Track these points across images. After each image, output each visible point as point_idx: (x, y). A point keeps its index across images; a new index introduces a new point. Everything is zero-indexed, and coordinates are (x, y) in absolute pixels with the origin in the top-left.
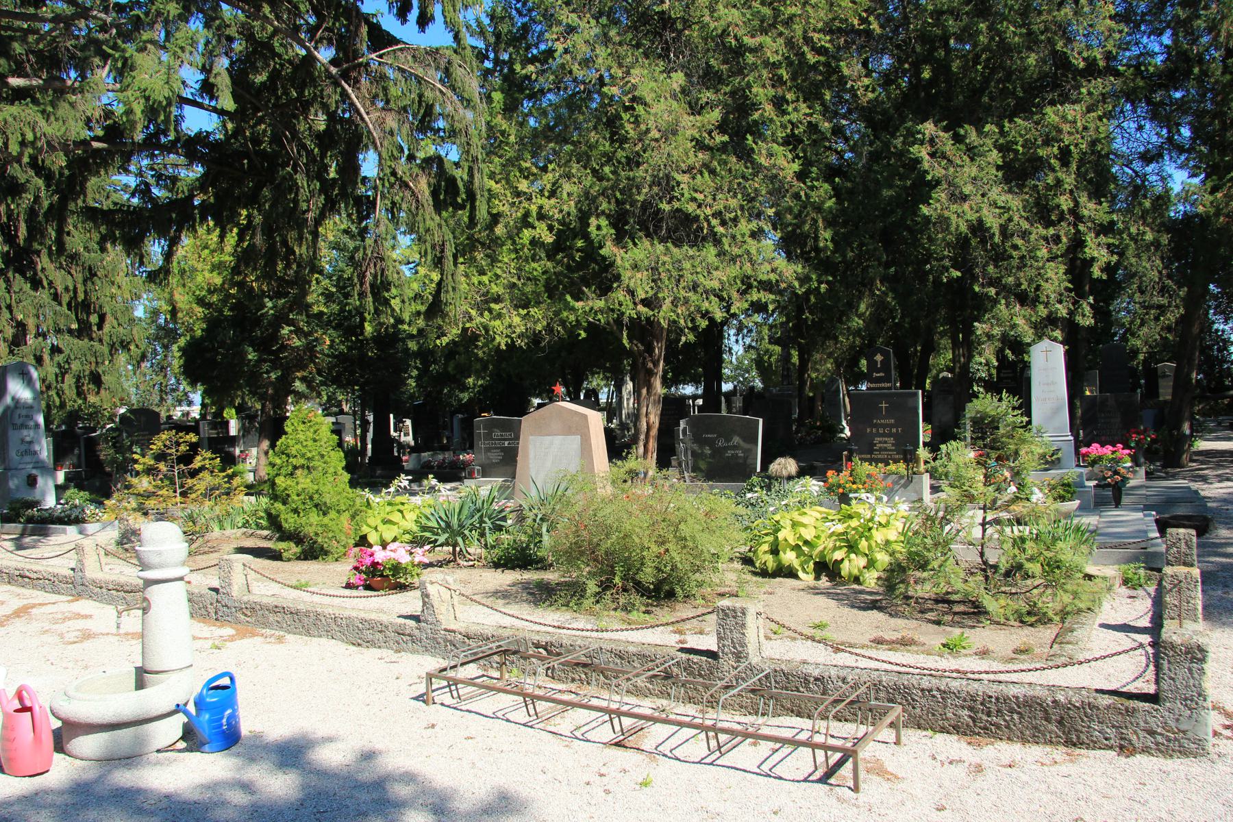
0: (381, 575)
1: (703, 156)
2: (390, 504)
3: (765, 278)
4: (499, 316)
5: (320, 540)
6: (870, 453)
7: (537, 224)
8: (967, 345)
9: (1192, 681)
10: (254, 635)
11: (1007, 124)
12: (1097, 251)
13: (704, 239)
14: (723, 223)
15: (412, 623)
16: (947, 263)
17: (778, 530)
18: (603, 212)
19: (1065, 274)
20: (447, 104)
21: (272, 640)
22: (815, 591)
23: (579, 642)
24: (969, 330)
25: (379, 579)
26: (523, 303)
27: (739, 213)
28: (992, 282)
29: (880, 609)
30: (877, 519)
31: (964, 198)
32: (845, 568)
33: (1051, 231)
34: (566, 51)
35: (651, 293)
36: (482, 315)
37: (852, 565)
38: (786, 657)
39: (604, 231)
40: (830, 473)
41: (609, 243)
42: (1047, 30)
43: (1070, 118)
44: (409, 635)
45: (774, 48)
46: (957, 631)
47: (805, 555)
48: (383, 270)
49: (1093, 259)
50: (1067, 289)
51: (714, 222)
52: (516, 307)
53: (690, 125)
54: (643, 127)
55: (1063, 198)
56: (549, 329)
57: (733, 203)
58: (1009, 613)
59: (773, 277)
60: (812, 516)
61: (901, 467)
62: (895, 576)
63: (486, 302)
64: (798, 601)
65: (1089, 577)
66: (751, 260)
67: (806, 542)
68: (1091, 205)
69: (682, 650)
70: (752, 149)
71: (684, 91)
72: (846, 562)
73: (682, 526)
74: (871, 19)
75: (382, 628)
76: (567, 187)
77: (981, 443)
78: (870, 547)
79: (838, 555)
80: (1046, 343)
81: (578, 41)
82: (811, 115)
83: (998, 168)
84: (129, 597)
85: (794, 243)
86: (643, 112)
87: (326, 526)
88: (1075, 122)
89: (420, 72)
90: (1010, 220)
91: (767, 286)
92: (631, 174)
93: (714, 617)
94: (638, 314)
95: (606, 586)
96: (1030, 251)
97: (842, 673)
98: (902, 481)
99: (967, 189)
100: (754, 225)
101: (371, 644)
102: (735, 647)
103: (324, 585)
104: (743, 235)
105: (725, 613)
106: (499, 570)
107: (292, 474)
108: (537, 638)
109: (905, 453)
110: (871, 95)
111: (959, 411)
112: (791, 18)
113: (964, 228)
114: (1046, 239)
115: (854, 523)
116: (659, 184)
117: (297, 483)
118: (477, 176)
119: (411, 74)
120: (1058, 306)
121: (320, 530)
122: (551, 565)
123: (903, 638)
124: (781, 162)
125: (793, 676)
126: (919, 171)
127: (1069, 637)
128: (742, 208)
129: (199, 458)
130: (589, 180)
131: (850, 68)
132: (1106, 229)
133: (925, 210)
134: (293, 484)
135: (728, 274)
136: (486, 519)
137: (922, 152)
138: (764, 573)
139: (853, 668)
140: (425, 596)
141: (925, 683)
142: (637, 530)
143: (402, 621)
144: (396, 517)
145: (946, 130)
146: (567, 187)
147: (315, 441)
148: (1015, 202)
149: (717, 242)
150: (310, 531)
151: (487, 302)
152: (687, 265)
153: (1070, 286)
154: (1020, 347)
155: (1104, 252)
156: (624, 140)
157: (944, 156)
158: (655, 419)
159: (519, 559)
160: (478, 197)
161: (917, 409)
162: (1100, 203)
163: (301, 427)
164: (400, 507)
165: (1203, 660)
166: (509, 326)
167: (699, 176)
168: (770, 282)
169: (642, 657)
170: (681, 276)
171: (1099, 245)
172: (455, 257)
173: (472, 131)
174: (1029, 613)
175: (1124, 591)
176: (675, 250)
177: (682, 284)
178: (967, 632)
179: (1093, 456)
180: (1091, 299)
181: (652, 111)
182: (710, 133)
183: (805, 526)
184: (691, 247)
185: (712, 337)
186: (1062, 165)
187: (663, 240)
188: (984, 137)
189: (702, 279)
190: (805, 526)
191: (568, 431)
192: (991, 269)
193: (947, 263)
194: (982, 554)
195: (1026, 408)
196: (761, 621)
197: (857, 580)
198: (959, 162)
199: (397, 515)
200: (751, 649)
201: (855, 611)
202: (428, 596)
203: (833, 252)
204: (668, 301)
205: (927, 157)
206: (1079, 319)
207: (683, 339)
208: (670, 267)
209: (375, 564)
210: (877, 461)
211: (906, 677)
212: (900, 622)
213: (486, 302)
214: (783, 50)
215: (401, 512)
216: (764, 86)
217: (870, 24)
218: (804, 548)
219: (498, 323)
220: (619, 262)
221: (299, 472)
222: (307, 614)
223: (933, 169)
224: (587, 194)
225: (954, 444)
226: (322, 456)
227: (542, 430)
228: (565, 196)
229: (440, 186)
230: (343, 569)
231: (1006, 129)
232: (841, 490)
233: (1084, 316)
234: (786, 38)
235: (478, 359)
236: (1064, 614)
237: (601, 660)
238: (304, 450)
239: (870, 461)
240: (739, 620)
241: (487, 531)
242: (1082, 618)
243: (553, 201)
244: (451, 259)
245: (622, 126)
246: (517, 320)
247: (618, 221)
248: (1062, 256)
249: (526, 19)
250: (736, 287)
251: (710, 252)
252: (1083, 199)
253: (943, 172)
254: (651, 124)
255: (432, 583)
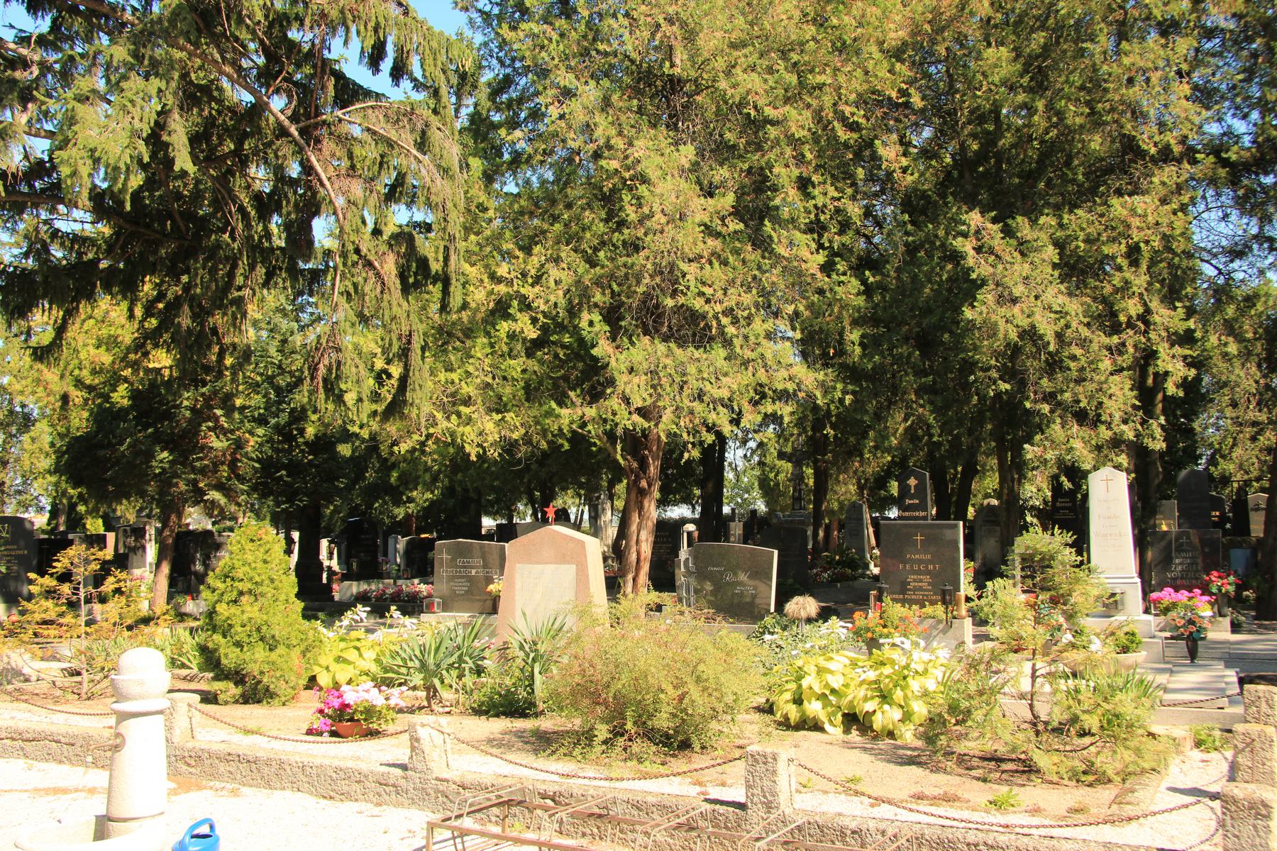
0: (351, 720)
1: (713, 243)
2: (342, 640)
3: (780, 387)
4: (469, 421)
5: (265, 680)
6: (904, 594)
7: (519, 315)
8: (1014, 470)
9: (1258, 841)
10: (200, 788)
11: (1066, 216)
12: (1173, 367)
13: (712, 339)
14: (735, 322)
15: (399, 772)
16: (995, 375)
17: (799, 678)
18: (596, 305)
19: (1131, 389)
20: (422, 171)
21: (224, 792)
22: (850, 746)
23: (591, 792)
24: (1018, 451)
25: (345, 722)
26: (499, 407)
27: (753, 310)
28: (1049, 397)
29: (919, 764)
30: (913, 666)
31: (1014, 301)
32: (878, 722)
33: (1115, 340)
34: (562, 117)
35: (649, 401)
36: (448, 418)
37: (886, 716)
38: (818, 810)
39: (597, 327)
40: (857, 615)
41: (601, 342)
42: (1112, 110)
43: (1139, 211)
44: (394, 786)
45: (799, 120)
46: (1004, 789)
47: (832, 705)
48: (339, 363)
49: (1167, 373)
50: (1134, 406)
51: (725, 321)
52: (490, 410)
53: (701, 209)
54: (646, 210)
55: (1131, 302)
56: (527, 439)
57: (747, 299)
58: (1063, 771)
59: (790, 387)
60: (839, 662)
61: (939, 610)
62: (933, 728)
63: (454, 402)
64: (832, 751)
65: (1151, 735)
66: (765, 366)
67: (833, 691)
68: (1164, 311)
69: (706, 800)
70: (770, 237)
71: (695, 167)
72: (879, 714)
73: (701, 667)
74: (912, 91)
75: (360, 778)
76: (554, 272)
77: (1029, 582)
78: (905, 697)
79: (869, 706)
80: (1106, 471)
81: (575, 108)
82: (839, 199)
83: (1055, 266)
84: (28, 746)
85: (817, 344)
86: (646, 193)
87: (273, 663)
88: (1145, 216)
89: (393, 135)
90: (1067, 326)
91: (783, 396)
92: (630, 260)
93: (741, 765)
94: (634, 425)
95: (618, 732)
96: (1092, 362)
97: (882, 826)
98: (941, 626)
99: (1018, 290)
100: (769, 325)
101: (347, 796)
102: (765, 797)
103: (282, 729)
104: (757, 337)
105: (754, 759)
106: (483, 718)
107: (235, 602)
108: (544, 787)
109: (944, 593)
110: (909, 178)
111: (1007, 543)
112: (820, 87)
113: (1013, 335)
114: (1109, 349)
115: (887, 670)
116: (661, 273)
117: (243, 612)
118: (453, 258)
119: (383, 136)
120: (1124, 427)
121: (266, 668)
122: (542, 713)
123: (946, 793)
124: (804, 253)
125: (828, 828)
126: (963, 268)
127: (1130, 797)
128: (757, 305)
129: (111, 579)
130: (582, 267)
131: (888, 151)
132: (1187, 338)
133: (968, 313)
134: (238, 613)
135: (741, 382)
136: (467, 659)
137: (966, 246)
138: (785, 724)
139: (893, 821)
140: (415, 740)
141: (971, 837)
142: (653, 669)
143: (386, 769)
144: (352, 655)
145: (994, 221)
146: (554, 272)
147: (265, 562)
148: (1074, 307)
149: (728, 343)
150: (253, 668)
151: (454, 404)
152: (692, 369)
153: (1137, 403)
154: (1077, 474)
155: (1180, 365)
156: (622, 224)
157: (991, 251)
158: (647, 549)
159: (510, 706)
160: (453, 281)
161: (957, 542)
162: (1175, 308)
163: (249, 546)
164: (357, 644)
165: (1267, 817)
166: (482, 433)
167: (708, 266)
168: (785, 391)
169: (663, 808)
170: (685, 382)
171: (1173, 357)
172: (423, 349)
173: (449, 205)
174: (1084, 773)
175: (1197, 754)
176: (678, 352)
177: (687, 391)
178: (1016, 789)
179: (1166, 602)
180: (1162, 420)
181: (658, 191)
182: (723, 219)
183: (831, 672)
184: (697, 348)
185: (714, 457)
186: (1131, 265)
187: (666, 339)
188: (1039, 231)
189: (708, 387)
190: (831, 672)
191: (562, 559)
192: (1045, 382)
193: (995, 375)
194: (1031, 706)
195: (1081, 544)
196: (793, 768)
197: (891, 734)
198: (1009, 259)
199: (355, 651)
200: (783, 798)
201: (892, 766)
202: (417, 740)
203: (861, 357)
204: (669, 411)
205: (972, 253)
206: (1147, 442)
207: (686, 455)
208: (673, 372)
209: (346, 706)
210: (911, 602)
211: (950, 830)
212: (941, 778)
213: (454, 402)
214: (809, 123)
215: (357, 649)
216: (787, 166)
217: (909, 95)
218: (831, 698)
219: (468, 429)
220: (613, 363)
221: (244, 599)
222: (268, 762)
223: (980, 267)
224: (578, 282)
225: (999, 582)
226: (272, 581)
227: (530, 558)
228: (552, 284)
229: (409, 267)
230: (306, 710)
231: (1065, 221)
232: (869, 635)
233: (1154, 439)
234: (815, 111)
235: (428, 469)
236: (1125, 775)
237: (617, 811)
238: (252, 574)
239: (903, 602)
240: (770, 766)
241: (467, 672)
242: (1145, 779)
243: (537, 289)
244: (419, 352)
245: (622, 208)
246: (490, 426)
247: (612, 316)
248: (1129, 369)
249: (509, 71)
250: (747, 397)
251: (719, 353)
252: (1154, 304)
253: (991, 270)
254: (656, 208)
255: (423, 725)
